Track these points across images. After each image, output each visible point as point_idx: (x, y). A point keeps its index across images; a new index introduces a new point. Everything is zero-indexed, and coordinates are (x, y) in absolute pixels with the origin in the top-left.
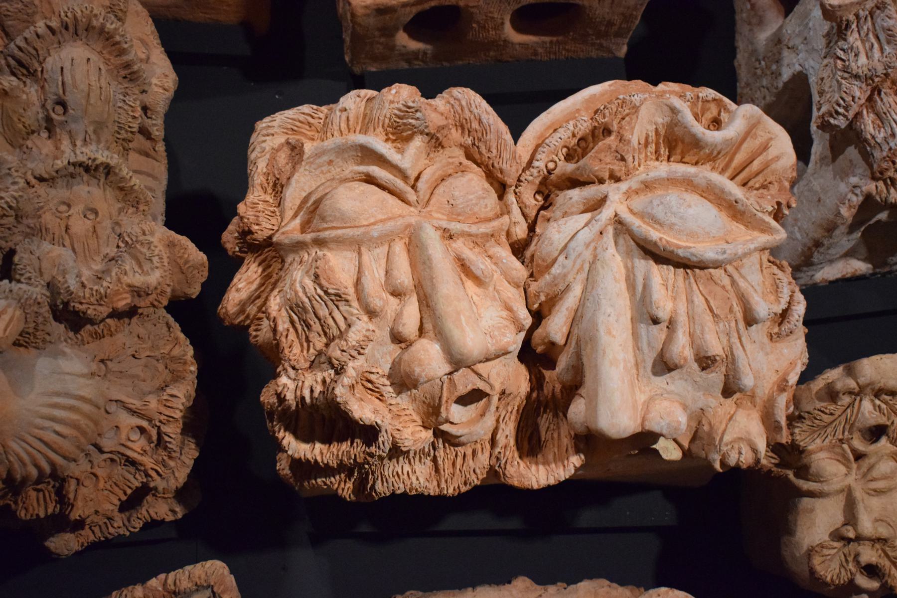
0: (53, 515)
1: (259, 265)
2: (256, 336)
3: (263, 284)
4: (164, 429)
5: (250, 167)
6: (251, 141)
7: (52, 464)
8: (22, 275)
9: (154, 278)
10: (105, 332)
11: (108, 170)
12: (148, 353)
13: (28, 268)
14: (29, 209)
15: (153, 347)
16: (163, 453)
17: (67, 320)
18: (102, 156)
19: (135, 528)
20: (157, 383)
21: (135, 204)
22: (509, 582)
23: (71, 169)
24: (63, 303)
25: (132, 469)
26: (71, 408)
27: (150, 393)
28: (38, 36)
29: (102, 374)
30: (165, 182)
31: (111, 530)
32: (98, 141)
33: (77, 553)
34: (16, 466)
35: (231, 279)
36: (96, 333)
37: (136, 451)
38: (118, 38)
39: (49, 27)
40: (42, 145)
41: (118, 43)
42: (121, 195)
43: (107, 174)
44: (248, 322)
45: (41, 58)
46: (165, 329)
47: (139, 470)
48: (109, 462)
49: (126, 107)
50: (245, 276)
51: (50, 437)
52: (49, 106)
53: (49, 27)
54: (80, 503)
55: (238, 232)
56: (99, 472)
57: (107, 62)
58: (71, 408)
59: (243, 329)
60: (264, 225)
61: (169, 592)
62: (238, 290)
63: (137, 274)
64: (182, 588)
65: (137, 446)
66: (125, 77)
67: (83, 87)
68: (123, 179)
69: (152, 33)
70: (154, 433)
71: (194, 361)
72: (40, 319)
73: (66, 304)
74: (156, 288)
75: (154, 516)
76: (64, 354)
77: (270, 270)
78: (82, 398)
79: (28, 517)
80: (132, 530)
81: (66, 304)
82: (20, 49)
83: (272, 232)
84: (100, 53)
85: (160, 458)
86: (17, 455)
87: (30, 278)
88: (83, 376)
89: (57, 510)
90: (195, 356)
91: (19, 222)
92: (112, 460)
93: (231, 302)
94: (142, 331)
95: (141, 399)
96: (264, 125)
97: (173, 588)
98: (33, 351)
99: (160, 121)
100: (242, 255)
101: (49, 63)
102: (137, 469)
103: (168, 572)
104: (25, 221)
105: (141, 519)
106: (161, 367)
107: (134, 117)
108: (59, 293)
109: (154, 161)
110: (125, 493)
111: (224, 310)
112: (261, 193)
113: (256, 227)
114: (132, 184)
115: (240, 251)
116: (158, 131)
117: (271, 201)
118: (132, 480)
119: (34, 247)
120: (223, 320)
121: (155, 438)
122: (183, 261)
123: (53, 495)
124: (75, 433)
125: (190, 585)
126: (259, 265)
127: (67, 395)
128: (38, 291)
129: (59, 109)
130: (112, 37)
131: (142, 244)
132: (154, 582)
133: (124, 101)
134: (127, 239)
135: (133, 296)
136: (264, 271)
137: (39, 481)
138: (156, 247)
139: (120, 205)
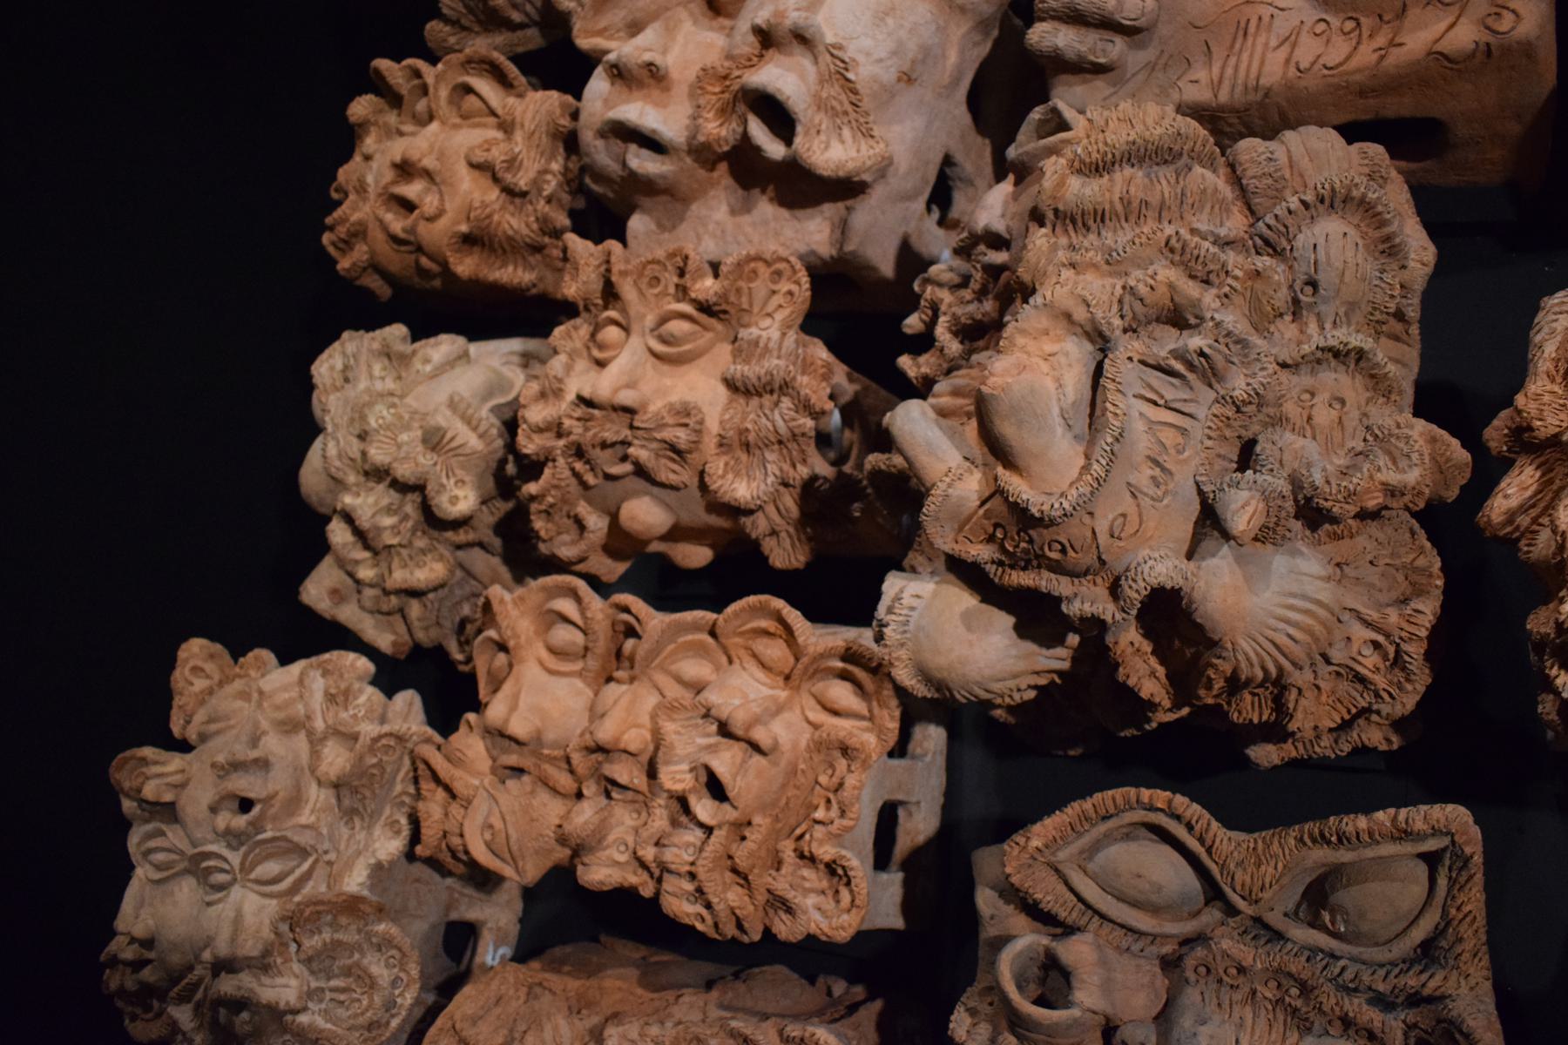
0: (1266, 722)
1: (1537, 469)
2: (1529, 552)
3: (1540, 492)
4: (1404, 646)
5: (1532, 351)
6: (1536, 321)
7: (1280, 669)
8: (1263, 466)
9: (1412, 476)
10: (1345, 533)
11: (1361, 354)
12: (1388, 561)
13: (1271, 459)
14: (1270, 396)
15: (1392, 555)
16: (1400, 676)
17: (1304, 517)
18: (1357, 340)
20: (1394, 595)
21: (1386, 393)
23: (1319, 354)
24: (1305, 498)
25: (1359, 687)
26: (1307, 612)
27: (1388, 605)
28: (1290, 212)
29: (1338, 578)
30: (1416, 370)
31: (1317, 749)
32: (1349, 324)
33: (1275, 767)
34: (1243, 665)
35: (1497, 483)
36: (1335, 533)
37: (1365, 667)
38: (1380, 208)
39: (1303, 202)
40: (1286, 329)
41: (1379, 214)
42: (1370, 383)
43: (1358, 361)
44: (1517, 534)
45: (1291, 236)
46: (1408, 535)
47: (1368, 689)
48: (1333, 676)
49: (1383, 285)
50: (1516, 481)
51: (1282, 639)
52: (1297, 288)
53: (1303, 202)
54: (1299, 715)
55: (1509, 428)
56: (1322, 684)
57: (1364, 236)
58: (1307, 612)
59: (1511, 543)
60: (1549, 420)
62: (1506, 497)
63: (1391, 472)
65: (1369, 662)
66: (1383, 252)
67: (1339, 264)
68: (1378, 364)
69: (1407, 201)
70: (1391, 650)
71: (1441, 574)
72: (1283, 514)
73: (1308, 500)
74: (1414, 488)
75: (1367, 742)
76: (1302, 554)
77: (1552, 475)
78: (1319, 603)
79: (1241, 721)
81: (1308, 500)
82: (1269, 227)
83: (1558, 429)
84: (1357, 226)
85: (1395, 680)
86: (1246, 654)
87: (1272, 470)
88: (1320, 578)
89: (1273, 718)
90: (1442, 569)
91: (1259, 411)
92: (1338, 674)
93: (1497, 511)
94: (1381, 536)
95: (1379, 611)
96: (1556, 301)
97: (1404, 825)
98: (1270, 547)
99: (1416, 301)
100: (1512, 456)
101: (1301, 240)
102: (1366, 687)
103: (1398, 807)
104: (1265, 410)
106: (1400, 577)
107: (1392, 296)
108: (1302, 488)
109: (1405, 347)
110: (1349, 711)
111: (1485, 519)
112: (1547, 381)
113: (1539, 423)
114: (1387, 370)
115: (1509, 450)
116: (1413, 312)
117: (1560, 392)
118: (1359, 698)
119: (1276, 438)
120: (1483, 530)
121: (1391, 656)
122: (1443, 459)
123: (1269, 702)
124: (1307, 638)
125: (1425, 827)
126: (1537, 469)
127: (1304, 597)
128: (1282, 485)
129: (1309, 290)
130: (1373, 208)
131: (1398, 438)
132: (1380, 815)
133: (1381, 278)
134: (1377, 432)
135: (1386, 495)
136: (1543, 475)
137: (1260, 685)
138: (1416, 441)
139: (1368, 394)
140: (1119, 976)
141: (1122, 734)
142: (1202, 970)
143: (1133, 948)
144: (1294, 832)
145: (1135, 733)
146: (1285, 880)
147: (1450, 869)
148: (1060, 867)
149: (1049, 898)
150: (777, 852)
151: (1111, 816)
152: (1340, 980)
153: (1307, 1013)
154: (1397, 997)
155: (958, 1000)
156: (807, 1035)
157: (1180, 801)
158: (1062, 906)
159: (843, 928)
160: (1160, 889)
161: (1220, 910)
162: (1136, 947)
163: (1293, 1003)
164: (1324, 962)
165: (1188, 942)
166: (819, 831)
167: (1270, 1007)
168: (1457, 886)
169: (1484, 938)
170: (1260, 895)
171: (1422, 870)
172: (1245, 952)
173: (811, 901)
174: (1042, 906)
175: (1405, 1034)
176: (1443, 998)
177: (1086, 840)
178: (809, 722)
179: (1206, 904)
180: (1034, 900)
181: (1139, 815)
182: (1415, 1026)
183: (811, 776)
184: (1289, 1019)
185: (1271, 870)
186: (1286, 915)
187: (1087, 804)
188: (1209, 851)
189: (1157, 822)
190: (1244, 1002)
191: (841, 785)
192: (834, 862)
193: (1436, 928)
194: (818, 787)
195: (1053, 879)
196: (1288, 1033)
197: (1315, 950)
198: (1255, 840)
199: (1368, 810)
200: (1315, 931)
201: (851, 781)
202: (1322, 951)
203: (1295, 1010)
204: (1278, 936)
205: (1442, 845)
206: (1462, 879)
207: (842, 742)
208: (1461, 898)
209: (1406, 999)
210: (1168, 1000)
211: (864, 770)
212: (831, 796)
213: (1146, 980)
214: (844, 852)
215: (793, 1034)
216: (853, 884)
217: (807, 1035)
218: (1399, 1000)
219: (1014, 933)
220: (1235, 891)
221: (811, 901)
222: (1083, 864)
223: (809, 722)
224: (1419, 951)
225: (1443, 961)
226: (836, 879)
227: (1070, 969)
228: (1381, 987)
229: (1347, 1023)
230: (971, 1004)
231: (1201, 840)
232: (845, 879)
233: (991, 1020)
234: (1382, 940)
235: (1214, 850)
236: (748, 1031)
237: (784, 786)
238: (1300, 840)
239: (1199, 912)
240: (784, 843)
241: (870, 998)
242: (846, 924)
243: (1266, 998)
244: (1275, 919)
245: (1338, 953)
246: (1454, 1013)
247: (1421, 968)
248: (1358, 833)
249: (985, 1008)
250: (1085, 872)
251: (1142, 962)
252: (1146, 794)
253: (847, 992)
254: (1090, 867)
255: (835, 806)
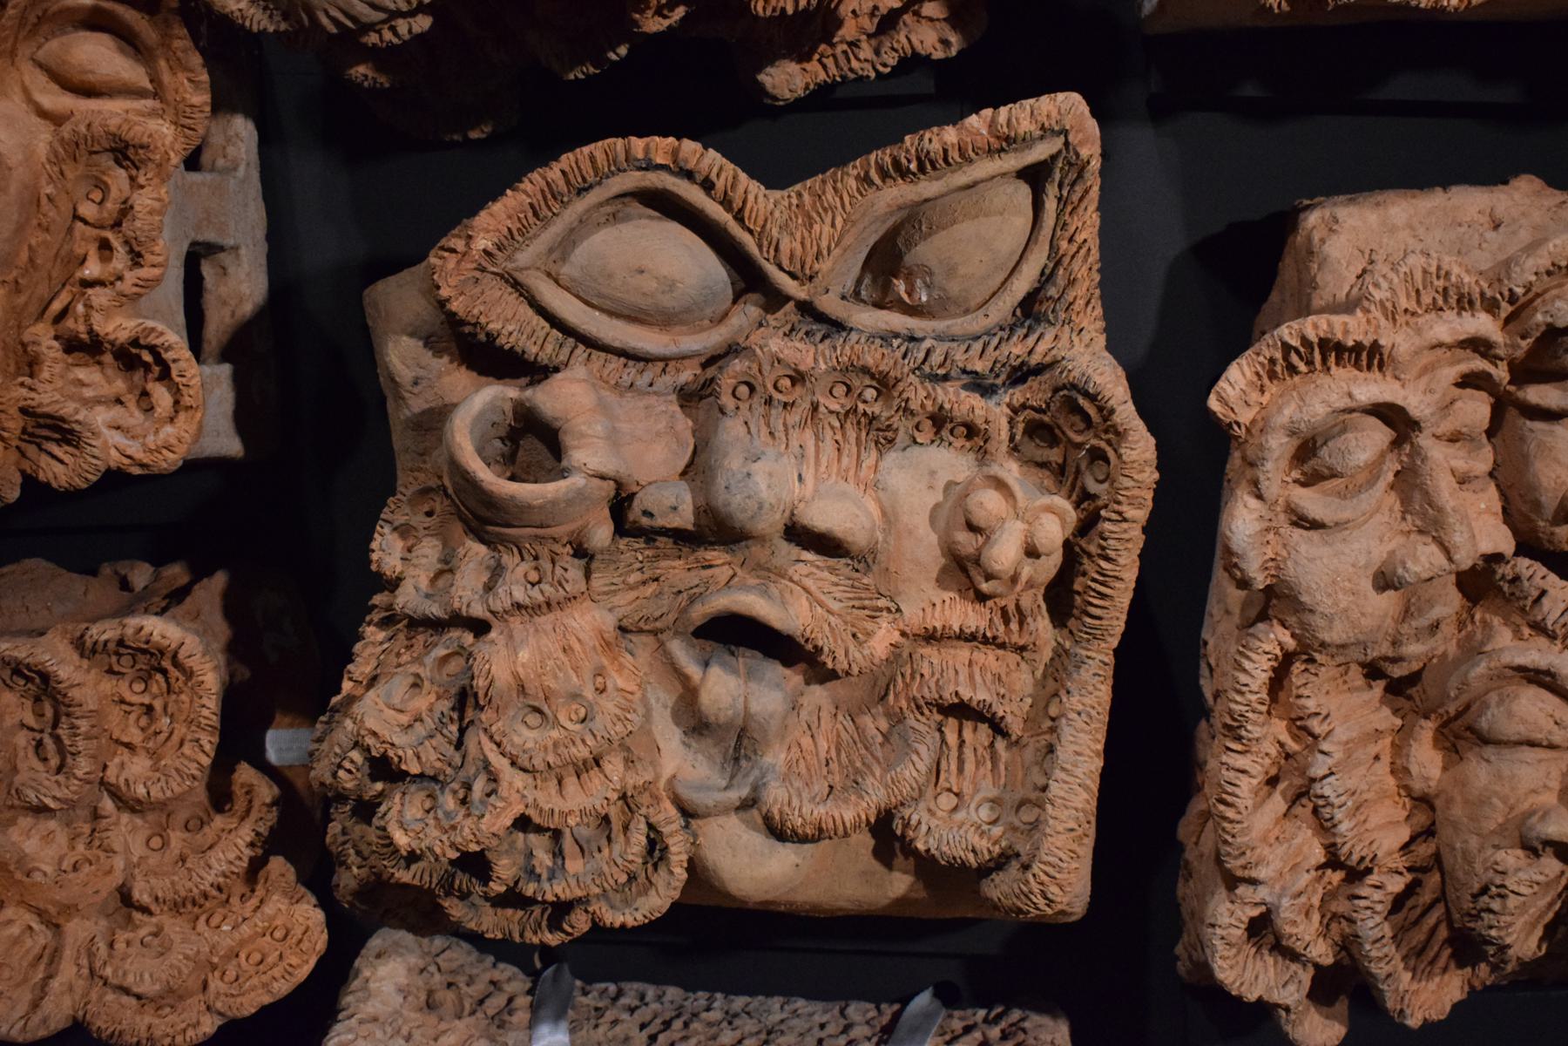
0: (806, 10)
19: (885, 65)
22: (1506, 182)
31: (854, 64)
61: (998, 138)
64: (1021, 132)
80: (881, 69)
103: (996, 107)
105: (896, 51)
125: (1033, 128)
132: (973, 121)
140: (624, 427)
141: (572, 77)
142: (744, 390)
143: (638, 383)
144: (854, 169)
145: (592, 70)
146: (848, 240)
147: (1060, 186)
148: (520, 277)
149: (511, 328)
150: (24, 345)
151: (591, 187)
152: (927, 369)
153: (888, 419)
154: (997, 376)
155: (377, 518)
156: (130, 631)
157: (690, 147)
158: (529, 338)
159: (169, 448)
160: (671, 285)
161: (756, 305)
162: (642, 382)
163: (869, 411)
164: (903, 349)
165: (713, 360)
166: (99, 296)
167: (837, 424)
168: (1069, 208)
169: (1097, 277)
170: (817, 266)
171: (1024, 192)
172: (803, 352)
173: (101, 417)
174: (502, 341)
175: (1011, 422)
176: (1054, 363)
177: (557, 228)
178: (43, 113)
179: (735, 302)
180: (488, 335)
181: (633, 180)
182: (1024, 406)
183: (66, 208)
184: (864, 434)
185: (827, 229)
186: (843, 298)
187: (554, 172)
188: (739, 217)
189: (660, 185)
190: (802, 425)
191: (126, 210)
192: (135, 342)
193: (1042, 274)
194: (79, 225)
195: (511, 298)
196: (864, 455)
197: (887, 337)
198: (799, 195)
199: (955, 119)
200: (884, 312)
201: (143, 201)
202: (897, 336)
203: (873, 419)
204: (838, 326)
205: (1054, 150)
206: (1075, 198)
207: (114, 136)
208: (1074, 223)
209: (1009, 377)
210: (695, 447)
211: (163, 181)
212: (109, 235)
213: (661, 426)
214: (150, 324)
215: (104, 637)
216: (174, 373)
217: (130, 631)
218: (999, 381)
219: (455, 401)
220: (781, 268)
221: (101, 417)
222: (553, 269)
223: (43, 113)
224: (1018, 312)
225: (1051, 317)
226: (138, 376)
227: (557, 424)
228: (979, 366)
229: (939, 420)
230: (400, 519)
231: (726, 203)
232: (157, 369)
233: (441, 534)
234: (973, 304)
235: (746, 214)
236: (21, 654)
237: (20, 229)
238: (866, 180)
239: (725, 315)
240: (32, 330)
241: (200, 572)
242: (173, 441)
243: (831, 412)
244: (830, 304)
245: (919, 334)
246: (1076, 373)
247: (1025, 331)
248: (945, 151)
249: (419, 520)
250: (557, 281)
251: (653, 400)
252: (638, 145)
253: (157, 577)
254: (566, 271)
255: (120, 251)
